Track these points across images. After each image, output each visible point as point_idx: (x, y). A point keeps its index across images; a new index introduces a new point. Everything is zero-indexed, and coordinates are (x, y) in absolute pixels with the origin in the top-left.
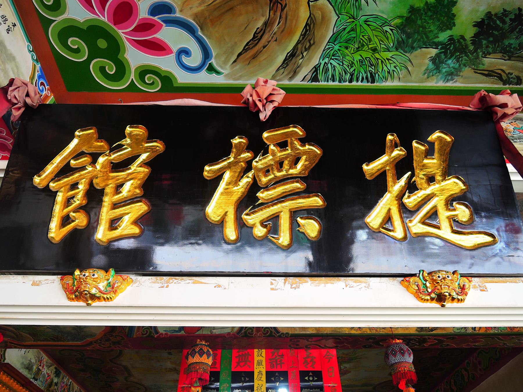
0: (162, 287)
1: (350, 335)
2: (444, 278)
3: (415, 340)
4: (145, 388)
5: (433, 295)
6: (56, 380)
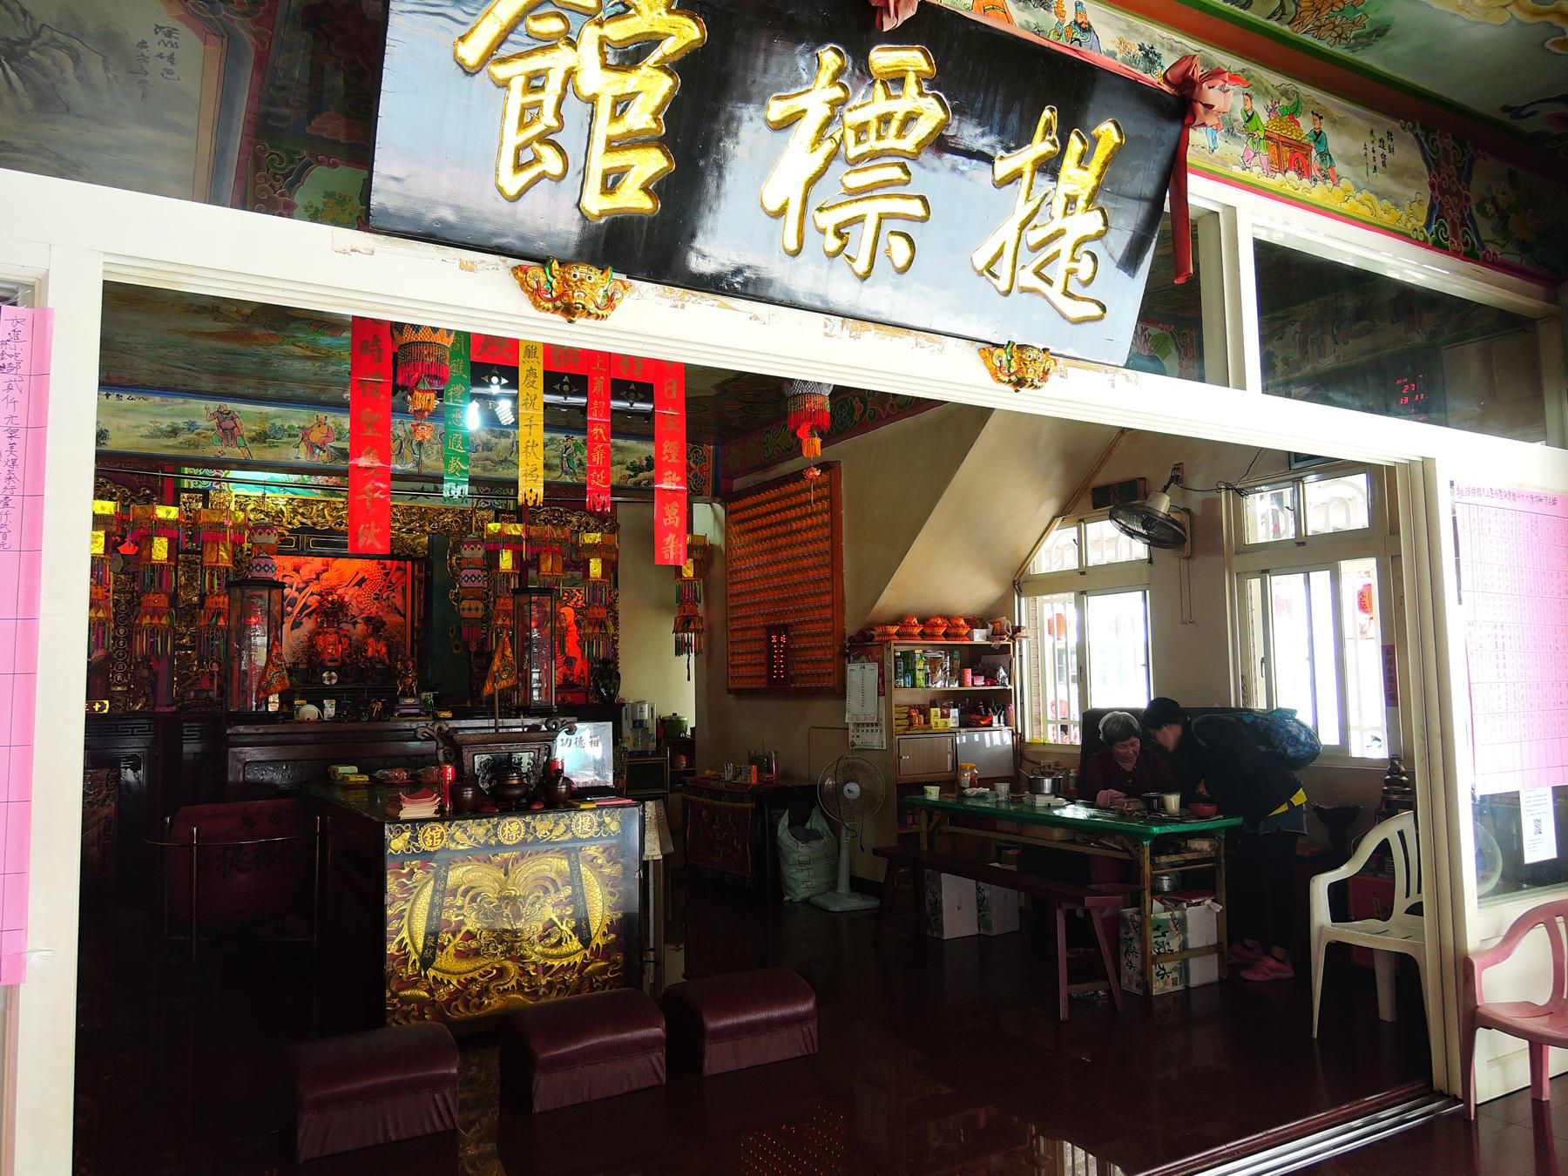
0: (676, 307)
2: (582, 280)
5: (558, 303)
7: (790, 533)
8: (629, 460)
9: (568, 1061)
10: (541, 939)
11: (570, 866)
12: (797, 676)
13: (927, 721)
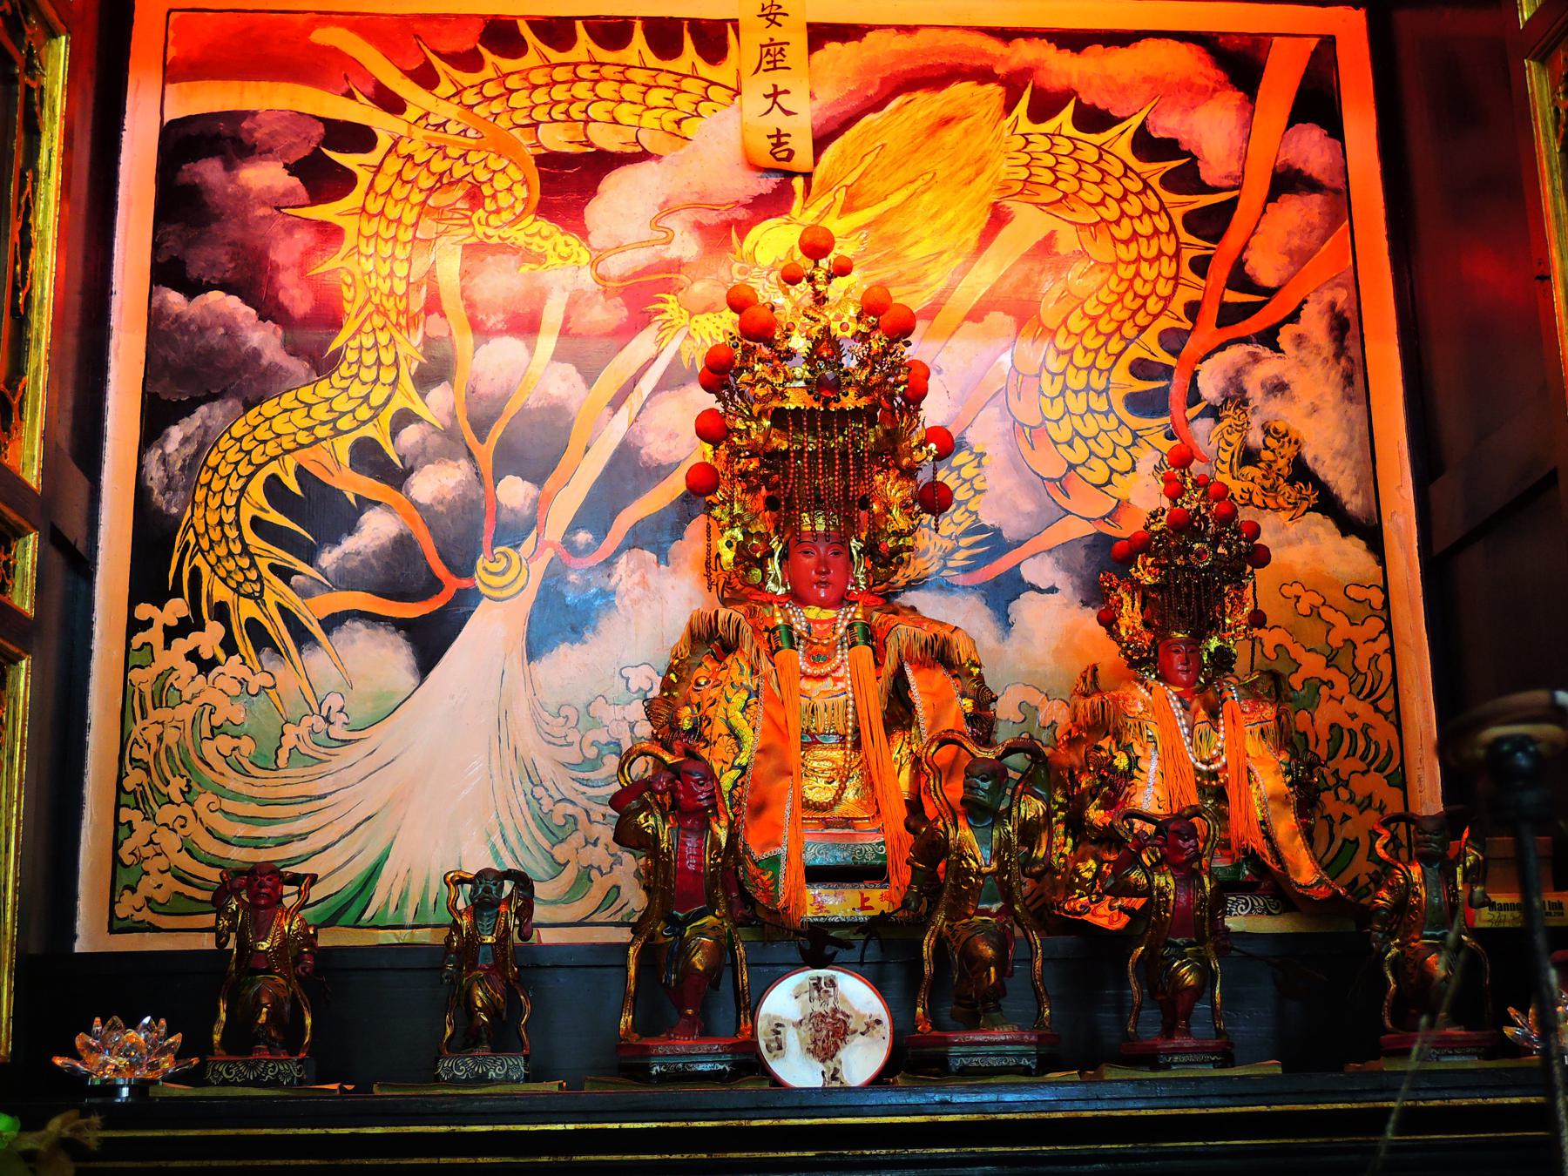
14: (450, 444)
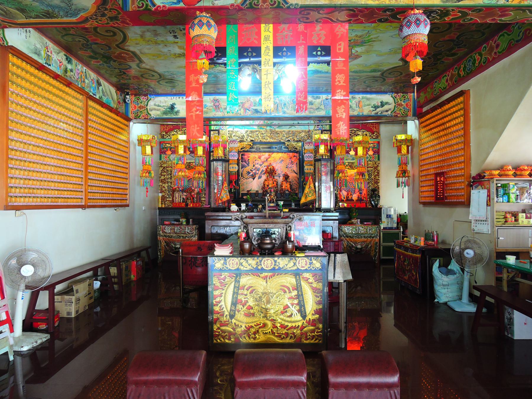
1: (366, 5)
3: (437, 13)
4: (159, 75)
6: (69, 67)
7: (446, 129)
8: (372, 104)
9: (253, 385)
10: (282, 313)
11: (296, 281)
12: (448, 196)
13: (516, 220)
14: (254, 169)
